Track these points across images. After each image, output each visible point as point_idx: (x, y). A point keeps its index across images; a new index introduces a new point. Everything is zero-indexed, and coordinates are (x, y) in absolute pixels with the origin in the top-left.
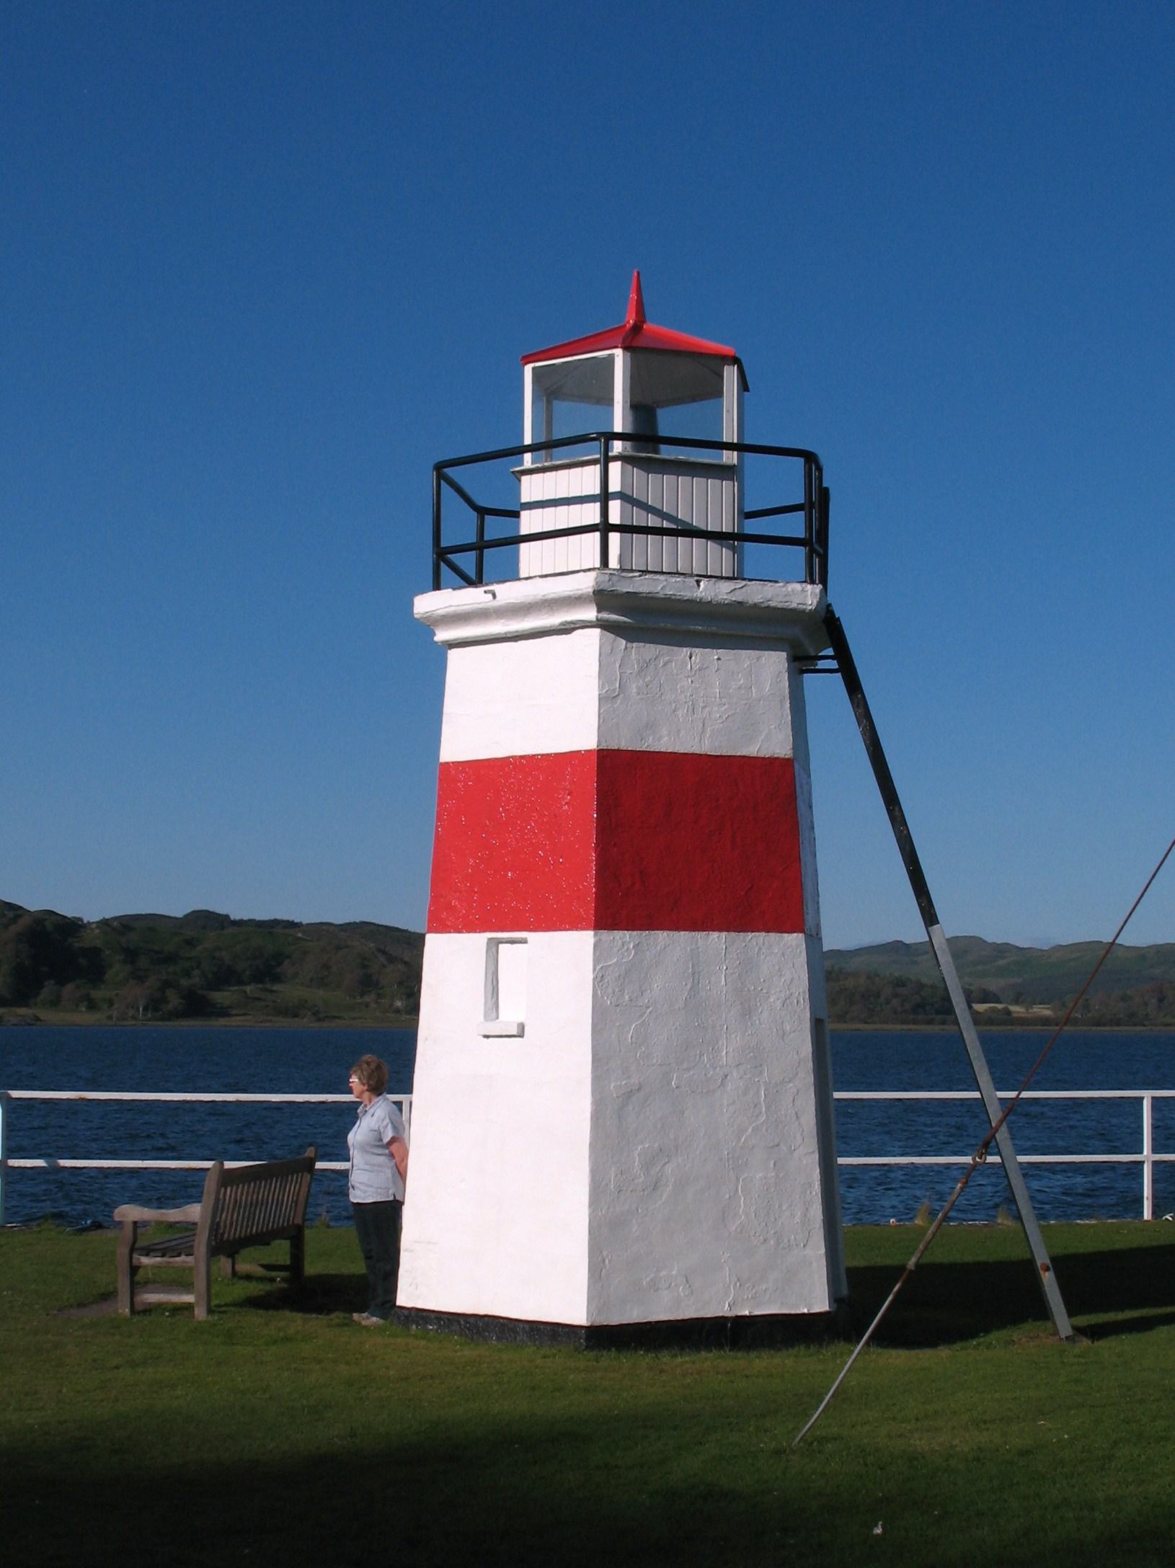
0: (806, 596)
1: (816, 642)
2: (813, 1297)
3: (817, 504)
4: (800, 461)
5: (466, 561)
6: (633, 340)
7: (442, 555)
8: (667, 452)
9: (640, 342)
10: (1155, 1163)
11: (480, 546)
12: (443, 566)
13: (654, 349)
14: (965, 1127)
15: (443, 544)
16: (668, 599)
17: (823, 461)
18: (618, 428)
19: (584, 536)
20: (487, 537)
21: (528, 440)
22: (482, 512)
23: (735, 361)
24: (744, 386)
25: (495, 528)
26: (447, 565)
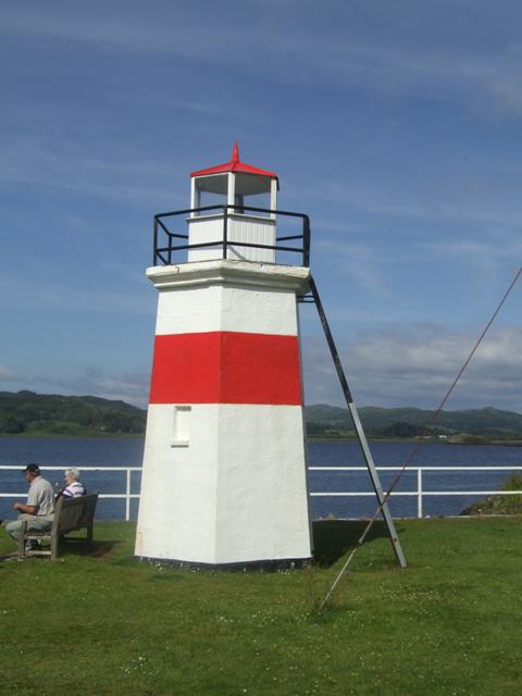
0: (303, 272)
1: (306, 290)
2: (302, 548)
3: (306, 236)
4: (302, 219)
5: (165, 255)
6: (235, 166)
7: (157, 252)
8: (247, 214)
9: (239, 169)
10: (423, 496)
11: (170, 249)
12: (158, 258)
14: (366, 481)
15: (159, 247)
16: (283, 276)
17: (311, 219)
20: (173, 246)
21: (192, 208)
22: (171, 235)
23: (276, 178)
24: (278, 189)
25: (176, 242)
26: (161, 255)
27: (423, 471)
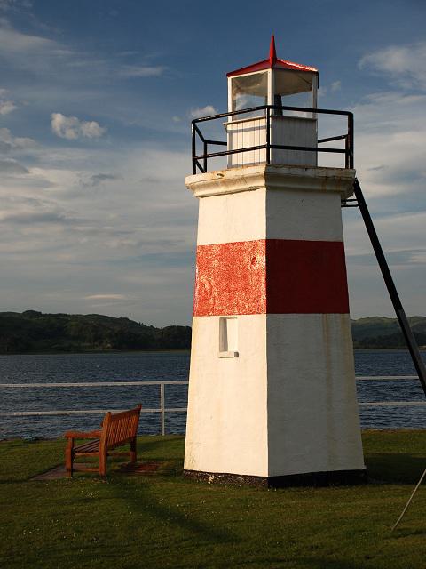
3: (350, 138)
6: (274, 63)
7: (195, 162)
11: (205, 157)
13: (249, 67)
17: (355, 119)
18: (269, 103)
19: (290, 151)
21: (230, 111)
22: (206, 142)
27: (166, 386)
